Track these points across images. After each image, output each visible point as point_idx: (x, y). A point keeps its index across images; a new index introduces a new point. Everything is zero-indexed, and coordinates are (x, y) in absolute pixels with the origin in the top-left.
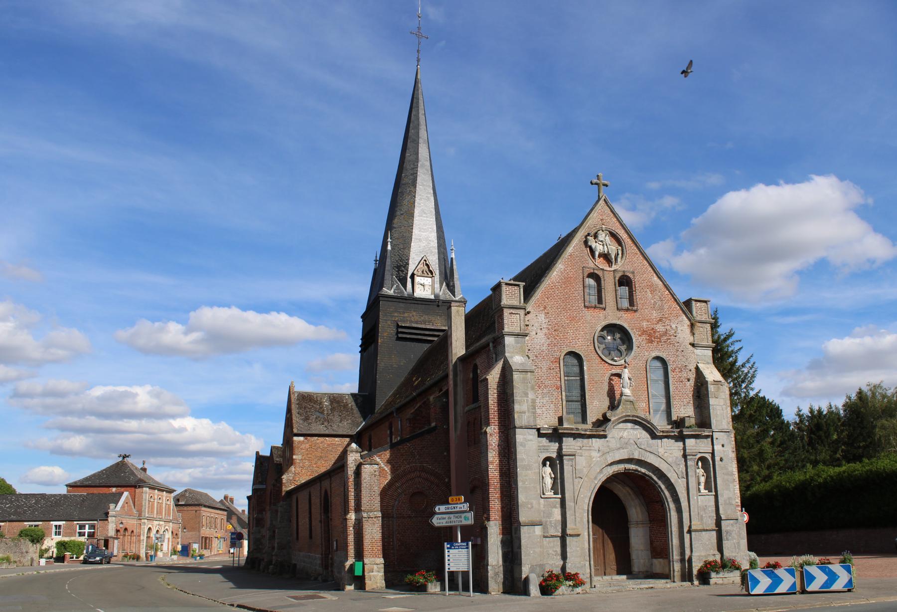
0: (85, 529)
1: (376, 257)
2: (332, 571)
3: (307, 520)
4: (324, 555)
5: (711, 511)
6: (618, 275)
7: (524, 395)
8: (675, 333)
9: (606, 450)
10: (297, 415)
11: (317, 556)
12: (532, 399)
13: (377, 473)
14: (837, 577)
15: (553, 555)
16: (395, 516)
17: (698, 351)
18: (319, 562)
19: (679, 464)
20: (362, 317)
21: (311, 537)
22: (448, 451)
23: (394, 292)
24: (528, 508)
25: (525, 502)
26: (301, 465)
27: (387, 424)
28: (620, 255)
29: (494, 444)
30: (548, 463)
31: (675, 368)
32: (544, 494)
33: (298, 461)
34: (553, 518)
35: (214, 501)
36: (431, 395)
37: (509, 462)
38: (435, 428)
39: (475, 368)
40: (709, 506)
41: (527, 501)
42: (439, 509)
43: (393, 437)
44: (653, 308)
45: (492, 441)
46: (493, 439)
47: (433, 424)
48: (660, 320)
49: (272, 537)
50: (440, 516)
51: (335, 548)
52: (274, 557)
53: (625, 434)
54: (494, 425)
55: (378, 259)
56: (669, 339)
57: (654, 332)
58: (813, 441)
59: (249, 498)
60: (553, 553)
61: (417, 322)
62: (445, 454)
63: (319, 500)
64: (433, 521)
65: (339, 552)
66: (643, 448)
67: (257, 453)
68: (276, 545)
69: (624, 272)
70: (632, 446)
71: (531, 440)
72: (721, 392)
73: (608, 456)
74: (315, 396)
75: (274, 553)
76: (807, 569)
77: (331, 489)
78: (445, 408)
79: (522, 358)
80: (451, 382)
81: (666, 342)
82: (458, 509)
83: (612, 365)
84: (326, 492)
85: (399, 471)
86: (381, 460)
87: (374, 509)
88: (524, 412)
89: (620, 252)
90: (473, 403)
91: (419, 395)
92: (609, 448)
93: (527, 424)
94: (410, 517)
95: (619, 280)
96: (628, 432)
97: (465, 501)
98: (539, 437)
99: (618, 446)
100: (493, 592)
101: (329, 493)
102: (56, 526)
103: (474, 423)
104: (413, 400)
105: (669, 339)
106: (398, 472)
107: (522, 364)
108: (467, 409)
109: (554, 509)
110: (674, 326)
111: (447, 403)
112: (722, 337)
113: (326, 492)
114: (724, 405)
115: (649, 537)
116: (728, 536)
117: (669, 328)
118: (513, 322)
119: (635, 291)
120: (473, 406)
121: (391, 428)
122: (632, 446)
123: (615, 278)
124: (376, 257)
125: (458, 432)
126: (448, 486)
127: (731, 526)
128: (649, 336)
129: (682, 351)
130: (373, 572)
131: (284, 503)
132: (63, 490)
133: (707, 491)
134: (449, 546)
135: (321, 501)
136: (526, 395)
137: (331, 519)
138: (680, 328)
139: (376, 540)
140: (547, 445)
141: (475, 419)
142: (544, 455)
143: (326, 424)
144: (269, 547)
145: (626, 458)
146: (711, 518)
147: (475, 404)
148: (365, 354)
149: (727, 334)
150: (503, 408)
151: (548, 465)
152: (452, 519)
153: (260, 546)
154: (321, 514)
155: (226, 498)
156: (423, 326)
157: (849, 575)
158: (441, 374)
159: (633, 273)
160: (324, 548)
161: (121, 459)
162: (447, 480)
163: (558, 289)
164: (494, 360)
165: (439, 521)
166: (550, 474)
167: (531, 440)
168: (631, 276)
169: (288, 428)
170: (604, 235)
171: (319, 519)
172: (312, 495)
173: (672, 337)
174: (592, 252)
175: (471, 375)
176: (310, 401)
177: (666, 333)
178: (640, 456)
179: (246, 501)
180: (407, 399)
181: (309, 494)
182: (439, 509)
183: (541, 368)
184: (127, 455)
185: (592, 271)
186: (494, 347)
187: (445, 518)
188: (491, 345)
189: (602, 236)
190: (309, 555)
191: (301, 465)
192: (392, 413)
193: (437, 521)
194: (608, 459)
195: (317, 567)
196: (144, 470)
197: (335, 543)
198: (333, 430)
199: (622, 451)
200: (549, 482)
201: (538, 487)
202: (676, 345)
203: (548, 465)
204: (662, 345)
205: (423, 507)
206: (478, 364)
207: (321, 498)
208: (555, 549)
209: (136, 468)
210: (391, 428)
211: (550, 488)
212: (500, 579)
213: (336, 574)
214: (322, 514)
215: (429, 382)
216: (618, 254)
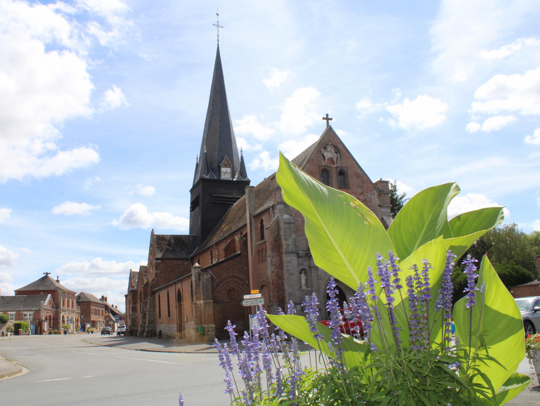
0: (27, 316)
1: (197, 156)
2: (184, 333)
3: (167, 306)
4: (178, 325)
6: (338, 170)
8: (370, 199)
10: (157, 248)
11: (174, 326)
12: (294, 238)
13: (210, 279)
16: (220, 302)
17: (383, 210)
18: (176, 329)
20: (190, 191)
21: (169, 315)
22: (248, 266)
23: (209, 177)
26: (160, 276)
27: (209, 252)
28: (339, 158)
30: (303, 272)
32: (301, 288)
33: (158, 274)
35: (97, 299)
36: (236, 236)
37: (282, 272)
38: (239, 255)
39: (262, 221)
42: (246, 297)
43: (213, 259)
44: (358, 187)
47: (239, 252)
48: (362, 193)
49: (144, 317)
50: (246, 301)
51: (186, 320)
52: (146, 328)
55: (198, 157)
59: (126, 296)
61: (223, 194)
62: (246, 268)
63: (174, 295)
64: (243, 303)
65: (188, 322)
67: (131, 270)
68: (147, 321)
69: (342, 167)
71: (294, 260)
74: (166, 237)
75: (146, 326)
77: (182, 289)
78: (245, 243)
79: (288, 216)
80: (248, 229)
82: (256, 297)
84: (179, 290)
88: (290, 245)
89: (339, 157)
90: (261, 240)
91: (229, 235)
93: (291, 251)
94: (228, 302)
95: (339, 172)
97: (259, 293)
98: (298, 257)
101: (181, 291)
102: (308, 288)
103: (262, 251)
104: (226, 238)
107: (288, 219)
108: (258, 243)
110: (369, 196)
111: (247, 240)
112: (399, 197)
113: (179, 290)
117: (366, 197)
119: (348, 178)
120: (261, 242)
121: (211, 254)
123: (337, 170)
124: (197, 156)
125: (253, 256)
126: (248, 285)
129: (374, 210)
131: (151, 297)
132: (13, 294)
134: (251, 316)
135: (176, 295)
136: (291, 235)
137: (183, 305)
138: (372, 198)
141: (263, 249)
142: (301, 268)
143: (173, 252)
144: (142, 323)
147: (262, 241)
148: (193, 212)
149: (402, 195)
151: (303, 273)
152: (253, 302)
153: (135, 323)
154: (176, 302)
155: (103, 297)
156: (226, 196)
158: (241, 224)
159: (347, 167)
160: (178, 321)
161: (45, 275)
162: (247, 282)
164: (273, 217)
165: (246, 303)
166: (304, 277)
167: (294, 260)
168: (345, 169)
169: (151, 255)
171: (175, 305)
172: (169, 292)
173: (369, 202)
175: (260, 225)
176: (163, 240)
179: (124, 298)
180: (221, 239)
181: (167, 292)
182: (246, 297)
184: (48, 273)
185: (324, 168)
186: (273, 210)
187: (249, 302)
188: (271, 209)
189: (329, 148)
190: (169, 326)
191: (160, 276)
192: (212, 246)
193: (245, 304)
195: (174, 332)
196: (58, 281)
197: (186, 318)
198: (177, 256)
200: (303, 281)
201: (298, 284)
202: (371, 206)
203: (303, 273)
206: (264, 219)
207: (176, 294)
209: (54, 280)
210: (211, 254)
211: (304, 285)
213: (187, 334)
214: (177, 303)
215: (234, 229)
216: (338, 158)
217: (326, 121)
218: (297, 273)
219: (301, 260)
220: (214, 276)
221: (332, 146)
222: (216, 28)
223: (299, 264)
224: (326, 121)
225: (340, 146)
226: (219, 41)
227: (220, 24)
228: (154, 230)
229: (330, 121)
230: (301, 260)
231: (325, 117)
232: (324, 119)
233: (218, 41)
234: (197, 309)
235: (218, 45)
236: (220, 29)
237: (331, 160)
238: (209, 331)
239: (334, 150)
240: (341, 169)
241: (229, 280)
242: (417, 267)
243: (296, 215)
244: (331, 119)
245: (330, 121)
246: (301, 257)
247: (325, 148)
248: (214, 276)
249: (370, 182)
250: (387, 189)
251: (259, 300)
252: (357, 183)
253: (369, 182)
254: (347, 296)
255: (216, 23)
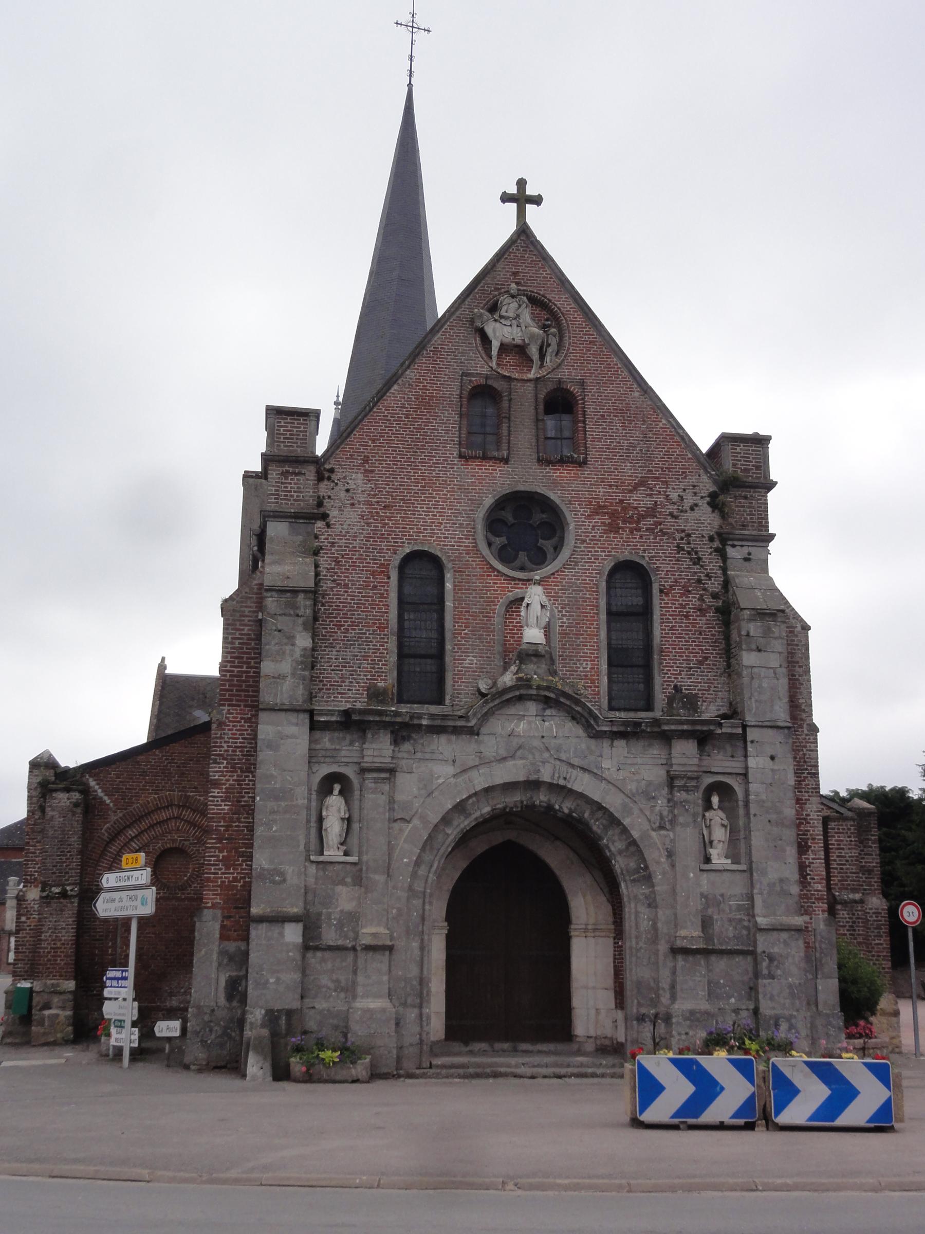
5: (734, 908)
7: (285, 641)
9: (472, 761)
14: (718, 1089)
15: (329, 988)
19: (654, 798)
24: (274, 882)
25: (267, 870)
29: (225, 745)
31: (671, 586)
34: (336, 908)
40: (731, 896)
41: (272, 867)
45: (221, 738)
46: (224, 734)
53: (522, 727)
54: (229, 705)
56: (660, 524)
57: (625, 509)
58: (517, 662)
60: (331, 985)
66: (564, 758)
70: (537, 755)
71: (293, 737)
72: (775, 638)
73: (474, 774)
76: (644, 1063)
81: (653, 529)
83: (514, 579)
85: (135, 806)
86: (98, 784)
87: (66, 880)
89: (554, 341)
92: (480, 758)
96: (529, 723)
99: (503, 753)
100: (194, 1065)
105: (660, 524)
106: (131, 809)
109: (340, 887)
110: (674, 496)
114: (781, 666)
115: (611, 960)
116: (773, 968)
118: (290, 492)
119: (584, 422)
122: (537, 755)
127: (782, 945)
128: (610, 518)
130: (50, 1008)
133: (729, 861)
139: (63, 944)
140: (333, 747)
142: (325, 770)
145: (522, 779)
146: (734, 924)
150: (236, 670)
151: (336, 792)
157: (750, 1085)
159: (582, 383)
163: (399, 420)
165: (112, 906)
166: (339, 811)
168: (575, 389)
170: (514, 305)
174: (486, 340)
177: (652, 512)
178: (556, 775)
183: (346, 586)
185: (483, 381)
189: (509, 307)
194: (476, 782)
199: (510, 763)
200: (334, 827)
203: (336, 792)
204: (641, 537)
205: (185, 878)
208: (334, 977)
212: (213, 1036)
217: (514, 206)
218: (302, 796)
219: (326, 740)
220: (106, 798)
221: (525, 299)
222: (404, 33)
223: (312, 758)
224: (514, 206)
225: (561, 302)
226: (415, 74)
227: (420, 21)
228: (166, 662)
229: (529, 207)
230: (326, 740)
231: (513, 190)
232: (506, 198)
233: (410, 76)
234: (23, 919)
235: (410, 85)
236: (420, 36)
237: (517, 351)
238: (47, 1006)
239: (534, 317)
240: (555, 390)
241: (164, 815)
242: (796, 781)
243: (337, 562)
244: (537, 200)
245: (529, 207)
246: (326, 726)
247: (493, 308)
248: (106, 798)
249: (683, 438)
250: (758, 468)
251: (140, 893)
252: (626, 443)
253: (677, 438)
254: (570, 898)
255: (406, 18)
